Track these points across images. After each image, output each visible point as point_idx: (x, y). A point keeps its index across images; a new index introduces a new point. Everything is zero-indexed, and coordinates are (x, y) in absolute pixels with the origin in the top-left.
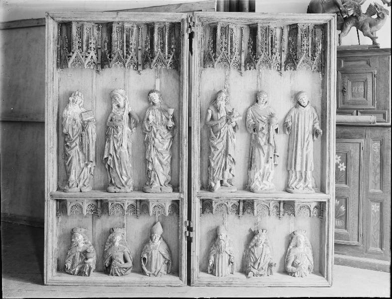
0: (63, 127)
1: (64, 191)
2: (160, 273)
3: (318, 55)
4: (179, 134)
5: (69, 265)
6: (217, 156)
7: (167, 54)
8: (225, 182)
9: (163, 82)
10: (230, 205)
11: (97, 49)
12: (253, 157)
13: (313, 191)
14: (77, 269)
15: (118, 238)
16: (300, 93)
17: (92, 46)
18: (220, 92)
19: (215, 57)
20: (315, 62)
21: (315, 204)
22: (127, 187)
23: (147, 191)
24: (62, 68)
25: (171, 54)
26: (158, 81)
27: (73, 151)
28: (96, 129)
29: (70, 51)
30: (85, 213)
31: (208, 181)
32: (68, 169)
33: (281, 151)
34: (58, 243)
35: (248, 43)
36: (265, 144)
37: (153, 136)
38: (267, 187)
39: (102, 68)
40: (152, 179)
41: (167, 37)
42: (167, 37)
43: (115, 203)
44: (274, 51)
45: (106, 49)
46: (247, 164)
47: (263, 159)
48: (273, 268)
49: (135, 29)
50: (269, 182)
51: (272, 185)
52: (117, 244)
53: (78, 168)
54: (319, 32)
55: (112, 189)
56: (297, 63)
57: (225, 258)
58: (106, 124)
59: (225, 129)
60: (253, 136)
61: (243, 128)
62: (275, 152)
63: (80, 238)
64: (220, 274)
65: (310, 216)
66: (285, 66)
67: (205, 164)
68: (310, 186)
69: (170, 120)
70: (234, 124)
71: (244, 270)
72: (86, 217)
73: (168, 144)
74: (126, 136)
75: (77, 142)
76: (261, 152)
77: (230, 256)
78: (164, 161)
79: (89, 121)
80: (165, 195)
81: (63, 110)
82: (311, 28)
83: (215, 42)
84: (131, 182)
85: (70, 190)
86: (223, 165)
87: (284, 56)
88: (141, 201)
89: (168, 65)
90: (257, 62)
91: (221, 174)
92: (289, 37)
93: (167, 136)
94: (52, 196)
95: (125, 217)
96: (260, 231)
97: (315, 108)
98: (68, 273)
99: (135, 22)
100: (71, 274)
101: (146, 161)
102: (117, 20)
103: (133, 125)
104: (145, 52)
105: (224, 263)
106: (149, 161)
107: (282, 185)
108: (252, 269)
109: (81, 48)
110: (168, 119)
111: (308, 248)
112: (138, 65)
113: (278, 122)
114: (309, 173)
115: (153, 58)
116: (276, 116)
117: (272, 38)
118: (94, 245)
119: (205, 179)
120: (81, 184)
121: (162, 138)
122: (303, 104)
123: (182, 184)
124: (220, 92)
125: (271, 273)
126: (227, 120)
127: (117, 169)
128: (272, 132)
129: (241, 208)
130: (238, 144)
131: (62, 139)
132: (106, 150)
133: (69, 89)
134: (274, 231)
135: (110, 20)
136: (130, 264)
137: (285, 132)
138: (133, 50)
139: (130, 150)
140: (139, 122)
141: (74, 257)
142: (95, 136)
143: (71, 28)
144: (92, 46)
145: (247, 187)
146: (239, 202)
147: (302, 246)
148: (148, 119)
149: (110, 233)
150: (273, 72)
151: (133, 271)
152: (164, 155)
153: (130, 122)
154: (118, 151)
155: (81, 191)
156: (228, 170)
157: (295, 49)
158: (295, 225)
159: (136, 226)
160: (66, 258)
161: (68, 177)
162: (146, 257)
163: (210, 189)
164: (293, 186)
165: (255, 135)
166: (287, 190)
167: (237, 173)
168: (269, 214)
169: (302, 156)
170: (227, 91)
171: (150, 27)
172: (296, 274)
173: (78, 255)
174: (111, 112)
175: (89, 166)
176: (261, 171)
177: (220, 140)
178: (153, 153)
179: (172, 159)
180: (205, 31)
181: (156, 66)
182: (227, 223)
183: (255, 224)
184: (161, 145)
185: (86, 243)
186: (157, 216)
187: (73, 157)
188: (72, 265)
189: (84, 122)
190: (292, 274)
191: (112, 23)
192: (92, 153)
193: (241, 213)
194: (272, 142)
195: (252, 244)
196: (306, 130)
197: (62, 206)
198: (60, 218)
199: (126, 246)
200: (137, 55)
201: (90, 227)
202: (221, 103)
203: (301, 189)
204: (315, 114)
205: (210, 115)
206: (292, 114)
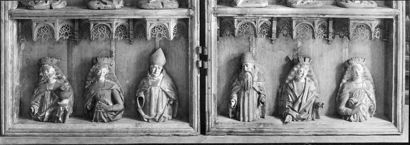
1: (28, 7)
2: (162, 118)
5: (35, 108)
10: (258, 26)
14: (47, 114)
15: (104, 71)
21: (376, 23)
48: (320, 110)
52: (102, 79)
57: (254, 96)
63: (51, 71)
64: (247, 119)
77: (259, 93)
85: (35, 7)
88: (134, 20)
95: (113, 43)
96: (302, 59)
100: (39, 121)
108: (291, 112)
111: (369, 82)
118: (69, 80)
125: (318, 117)
129: (274, 29)
136: (121, 106)
141: (43, 97)
151: (124, 116)
158: (350, 51)
159: (128, 54)
168: (314, 37)
173: (48, 95)
183: (294, 50)
185: (59, 78)
190: (346, 117)
195: (290, 78)
199: (115, 81)
201: (65, 56)
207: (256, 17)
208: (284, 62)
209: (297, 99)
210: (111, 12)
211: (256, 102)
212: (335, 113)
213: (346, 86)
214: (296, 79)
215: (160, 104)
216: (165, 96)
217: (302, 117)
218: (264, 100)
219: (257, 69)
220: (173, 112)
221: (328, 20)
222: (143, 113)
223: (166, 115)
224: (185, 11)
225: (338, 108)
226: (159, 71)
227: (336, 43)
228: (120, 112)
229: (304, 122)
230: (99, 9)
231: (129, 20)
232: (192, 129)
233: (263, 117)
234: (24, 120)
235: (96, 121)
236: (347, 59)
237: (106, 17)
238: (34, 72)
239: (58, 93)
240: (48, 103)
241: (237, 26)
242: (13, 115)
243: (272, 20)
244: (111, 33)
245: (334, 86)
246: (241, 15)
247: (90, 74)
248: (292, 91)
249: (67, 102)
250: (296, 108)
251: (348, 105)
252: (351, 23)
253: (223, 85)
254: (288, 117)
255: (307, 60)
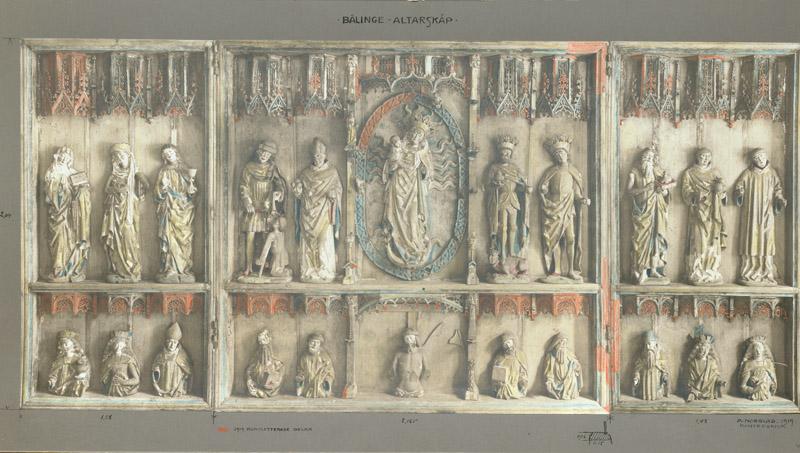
0: (45, 194)
1: (48, 281)
2: (177, 394)
3: (779, 102)
4: (204, 204)
5: (53, 381)
6: (643, 234)
7: (186, 95)
8: (654, 271)
9: (181, 134)
10: (660, 303)
11: (90, 89)
12: (692, 237)
13: (775, 283)
14: (64, 388)
15: (121, 345)
16: (114, 145)
17: (84, 85)
18: (647, 149)
19: (640, 102)
20: (777, 108)
21: (777, 301)
22: (133, 276)
23: (161, 280)
24: (44, 115)
25: (135, 96)
26: (174, 133)
27: (60, 227)
28: (91, 199)
29: (54, 93)
30: (76, 311)
31: (630, 272)
32: (53, 251)
33: (730, 228)
34: (40, 352)
35: (685, 83)
36: (708, 219)
37: (168, 205)
38: (711, 279)
39: (98, 115)
40: (167, 264)
41: (185, 72)
42: (185, 72)
43: (315, 298)
44: (721, 92)
45: (103, 89)
46: (684, 248)
47: (705, 240)
48: (722, 389)
49: (142, 61)
50: (714, 269)
51: (719, 275)
52: (119, 353)
53: (67, 251)
54: (582, 66)
55: (113, 278)
56: (753, 110)
57: (656, 375)
58: (104, 190)
59: (653, 199)
60: (692, 209)
61: (678, 199)
62: (722, 230)
63: (69, 345)
64: (650, 397)
65: (771, 317)
66: (735, 114)
67: (626, 246)
68: (771, 276)
69: (192, 185)
70: (666, 192)
71: (682, 390)
72: (77, 316)
73: (188, 216)
74: (132, 205)
75: (65, 214)
76: (703, 231)
77: (661, 371)
78: (183, 239)
79: (81, 186)
80: (185, 286)
81: (45, 172)
82: (772, 60)
83: (639, 82)
84: (138, 269)
85: (55, 280)
86: (650, 249)
87: (734, 101)
88: (151, 294)
89: (188, 111)
90: (696, 109)
91: (648, 260)
92: (740, 75)
93: (188, 206)
94: (31, 288)
95: (130, 317)
96: (703, 337)
97: (777, 170)
98: (50, 393)
99: (141, 51)
100: (56, 394)
101: (160, 241)
102: (117, 48)
103: (140, 192)
104: (157, 93)
105: (653, 382)
106: (163, 241)
107: (731, 274)
108: (693, 390)
109: (69, 87)
110: (189, 183)
111: (769, 360)
112: (147, 111)
113: (725, 189)
114: (769, 259)
115: (167, 101)
116: (723, 181)
117: (718, 76)
118: (87, 354)
119: (625, 268)
120: (70, 272)
121: (181, 209)
122: (760, 165)
123: (208, 271)
124: (647, 149)
125: (720, 396)
126: (656, 188)
127: (120, 251)
128: (718, 203)
129: (676, 307)
130: (671, 223)
131: (44, 209)
132: (105, 225)
133: (53, 143)
134: (723, 339)
135: (108, 49)
136: (136, 380)
137: (735, 204)
138: (140, 90)
139: (137, 225)
140: (148, 186)
141: (61, 370)
142: (89, 207)
143: (55, 61)
144: (84, 85)
145: (684, 277)
146: (673, 298)
147: (760, 358)
148: (161, 184)
149: (111, 338)
150: (719, 124)
151: (140, 391)
152: (184, 232)
153: (136, 189)
154: (121, 227)
155: (70, 281)
156: (657, 255)
157: (749, 92)
158: (750, 330)
159: (145, 328)
160: (49, 373)
161: (53, 261)
162: (158, 370)
163: (635, 281)
164: (747, 276)
165: (695, 208)
166: (739, 280)
167: (668, 258)
168: (715, 316)
169: (759, 235)
170: (656, 149)
171: (162, 58)
172: (753, 396)
173: (65, 368)
174: (111, 174)
175: (82, 248)
176: (703, 256)
177: (645, 215)
178: (169, 228)
179: (194, 237)
180: (625, 66)
181: (172, 112)
182: (656, 328)
183: (696, 329)
184: (179, 218)
185: (77, 352)
186: (174, 314)
187: (59, 235)
188: (58, 383)
189: (74, 187)
190: (747, 396)
191: (110, 53)
192: (86, 229)
193: (676, 314)
194: (717, 217)
195: (692, 356)
196: (765, 200)
197: (45, 303)
198: (42, 318)
199: (132, 355)
200: (145, 96)
201: (83, 330)
202: (648, 165)
203: (758, 280)
204: (777, 179)
205: (633, 180)
206: (746, 179)
207: (659, 294)
208: (685, 340)
209: (699, 378)
210: (129, 285)
211: (658, 380)
212: (737, 391)
213: (747, 364)
214: (698, 357)
215: (175, 379)
216: (180, 372)
217: (704, 395)
218: (666, 378)
219: (660, 348)
220: (188, 388)
221: (729, 298)
222: (158, 388)
223: (181, 389)
224: (202, 285)
225: (739, 386)
226: (175, 345)
227: (737, 322)
228: (136, 386)
229: (706, 401)
230: (117, 283)
231: (146, 294)
232: (205, 404)
233: (665, 396)
234: (40, 394)
235: (112, 395)
236: (748, 337)
237: (124, 291)
238: (52, 347)
239: (75, 366)
240: (66, 376)
241: (639, 304)
242: (30, 389)
243: (673, 298)
244: (128, 307)
245: (735, 364)
246: (643, 293)
247: (107, 348)
248: (694, 369)
249: (84, 376)
250: (698, 387)
251: (749, 384)
252: (752, 301)
253: (626, 363)
254: (691, 395)
255: (709, 338)
